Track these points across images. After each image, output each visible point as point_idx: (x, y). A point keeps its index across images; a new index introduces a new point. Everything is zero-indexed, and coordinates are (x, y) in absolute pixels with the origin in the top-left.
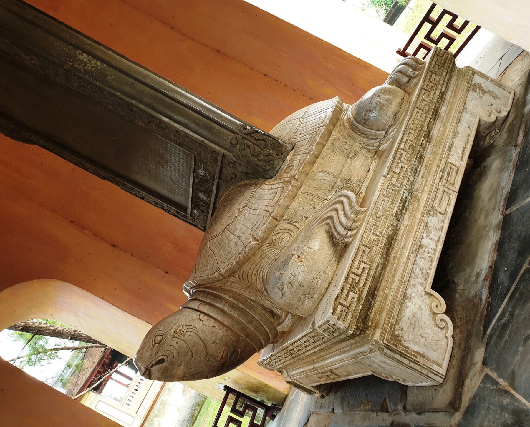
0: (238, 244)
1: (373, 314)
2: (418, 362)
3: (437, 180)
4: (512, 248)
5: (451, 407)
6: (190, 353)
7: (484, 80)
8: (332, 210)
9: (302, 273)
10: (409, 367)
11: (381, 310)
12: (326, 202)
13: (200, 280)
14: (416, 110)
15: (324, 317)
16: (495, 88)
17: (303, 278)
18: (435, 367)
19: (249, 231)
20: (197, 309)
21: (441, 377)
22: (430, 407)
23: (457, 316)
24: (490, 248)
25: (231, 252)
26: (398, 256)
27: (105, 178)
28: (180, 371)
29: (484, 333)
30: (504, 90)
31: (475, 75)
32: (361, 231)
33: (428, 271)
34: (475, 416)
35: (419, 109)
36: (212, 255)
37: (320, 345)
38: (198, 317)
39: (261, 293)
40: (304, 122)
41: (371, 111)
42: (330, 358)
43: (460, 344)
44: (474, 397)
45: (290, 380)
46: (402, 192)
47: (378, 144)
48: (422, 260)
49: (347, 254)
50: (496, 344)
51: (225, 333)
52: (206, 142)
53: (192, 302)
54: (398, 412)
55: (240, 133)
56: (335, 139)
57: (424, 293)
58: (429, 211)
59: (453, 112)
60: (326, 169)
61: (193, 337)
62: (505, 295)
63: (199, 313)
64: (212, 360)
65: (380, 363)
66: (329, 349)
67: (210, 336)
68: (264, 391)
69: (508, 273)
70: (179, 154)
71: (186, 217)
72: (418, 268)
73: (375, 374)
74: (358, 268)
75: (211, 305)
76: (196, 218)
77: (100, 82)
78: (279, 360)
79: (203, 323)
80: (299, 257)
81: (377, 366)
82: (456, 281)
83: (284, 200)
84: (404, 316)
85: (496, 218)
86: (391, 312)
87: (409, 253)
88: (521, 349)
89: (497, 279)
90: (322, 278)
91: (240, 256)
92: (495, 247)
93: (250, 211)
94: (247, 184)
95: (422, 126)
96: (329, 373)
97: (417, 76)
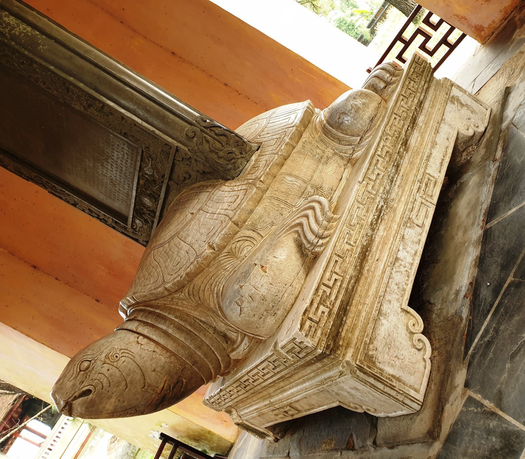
0: (190, 252)
1: (344, 331)
2: (393, 386)
3: (415, 191)
4: (494, 263)
5: (430, 436)
6: (124, 382)
7: (462, 93)
8: (302, 216)
9: (265, 284)
10: (383, 393)
11: (353, 330)
12: (294, 209)
13: (140, 296)
14: (394, 116)
15: (290, 334)
16: (472, 103)
17: (266, 291)
18: (412, 393)
19: (204, 238)
20: (135, 330)
21: (418, 404)
22: (404, 439)
23: (434, 336)
24: (469, 264)
25: (181, 263)
26: (372, 269)
27: (28, 179)
28: (110, 405)
29: (466, 353)
30: (481, 105)
31: (453, 87)
32: (334, 240)
33: (405, 287)
34: (458, 444)
35: (396, 115)
36: (157, 266)
37: (281, 371)
38: (136, 339)
39: (214, 312)
40: (271, 122)
41: (345, 114)
42: (290, 388)
43: (439, 367)
44: (456, 423)
45: (240, 421)
46: (377, 201)
47: (352, 151)
48: (398, 273)
49: (317, 265)
50: (479, 364)
51: (168, 360)
52: (157, 132)
53: (129, 322)
54: (367, 449)
55: (199, 126)
56: (306, 141)
57: (400, 310)
58: (406, 223)
59: (432, 122)
60: (296, 173)
61: (129, 363)
62: (489, 311)
63: (137, 335)
64: (151, 392)
65: (349, 390)
66: (290, 377)
67: (149, 362)
68: (206, 439)
69: (491, 288)
70: (123, 148)
71: (125, 228)
72: (394, 283)
73: (342, 405)
74: (329, 280)
75: (152, 326)
76: (137, 230)
77: (29, 51)
78: (228, 395)
79: (142, 347)
80: (262, 267)
81: (346, 394)
82: (432, 301)
83: (247, 203)
84: (378, 334)
85: (476, 233)
86: (364, 330)
87: (384, 266)
88: (508, 365)
89: (479, 295)
90: (288, 292)
91: (192, 266)
92: (476, 263)
93: (206, 215)
94: (204, 186)
95: (400, 133)
96: (288, 408)
97: (394, 83)
